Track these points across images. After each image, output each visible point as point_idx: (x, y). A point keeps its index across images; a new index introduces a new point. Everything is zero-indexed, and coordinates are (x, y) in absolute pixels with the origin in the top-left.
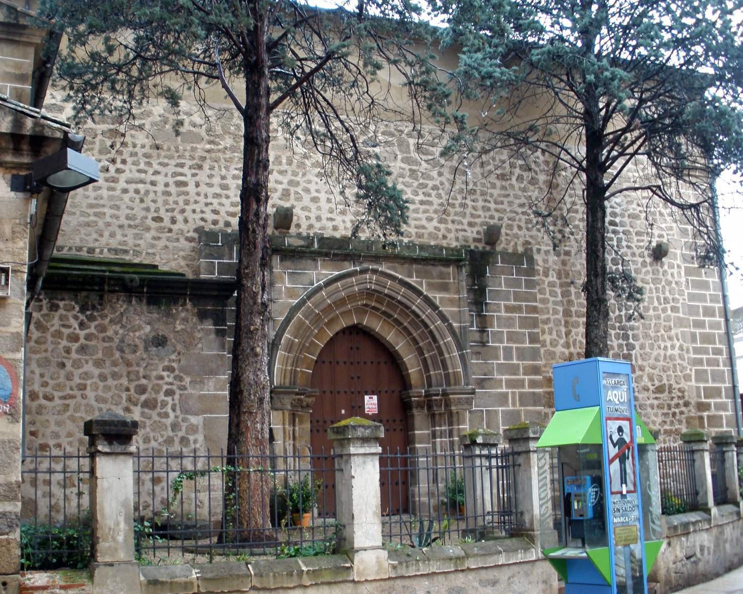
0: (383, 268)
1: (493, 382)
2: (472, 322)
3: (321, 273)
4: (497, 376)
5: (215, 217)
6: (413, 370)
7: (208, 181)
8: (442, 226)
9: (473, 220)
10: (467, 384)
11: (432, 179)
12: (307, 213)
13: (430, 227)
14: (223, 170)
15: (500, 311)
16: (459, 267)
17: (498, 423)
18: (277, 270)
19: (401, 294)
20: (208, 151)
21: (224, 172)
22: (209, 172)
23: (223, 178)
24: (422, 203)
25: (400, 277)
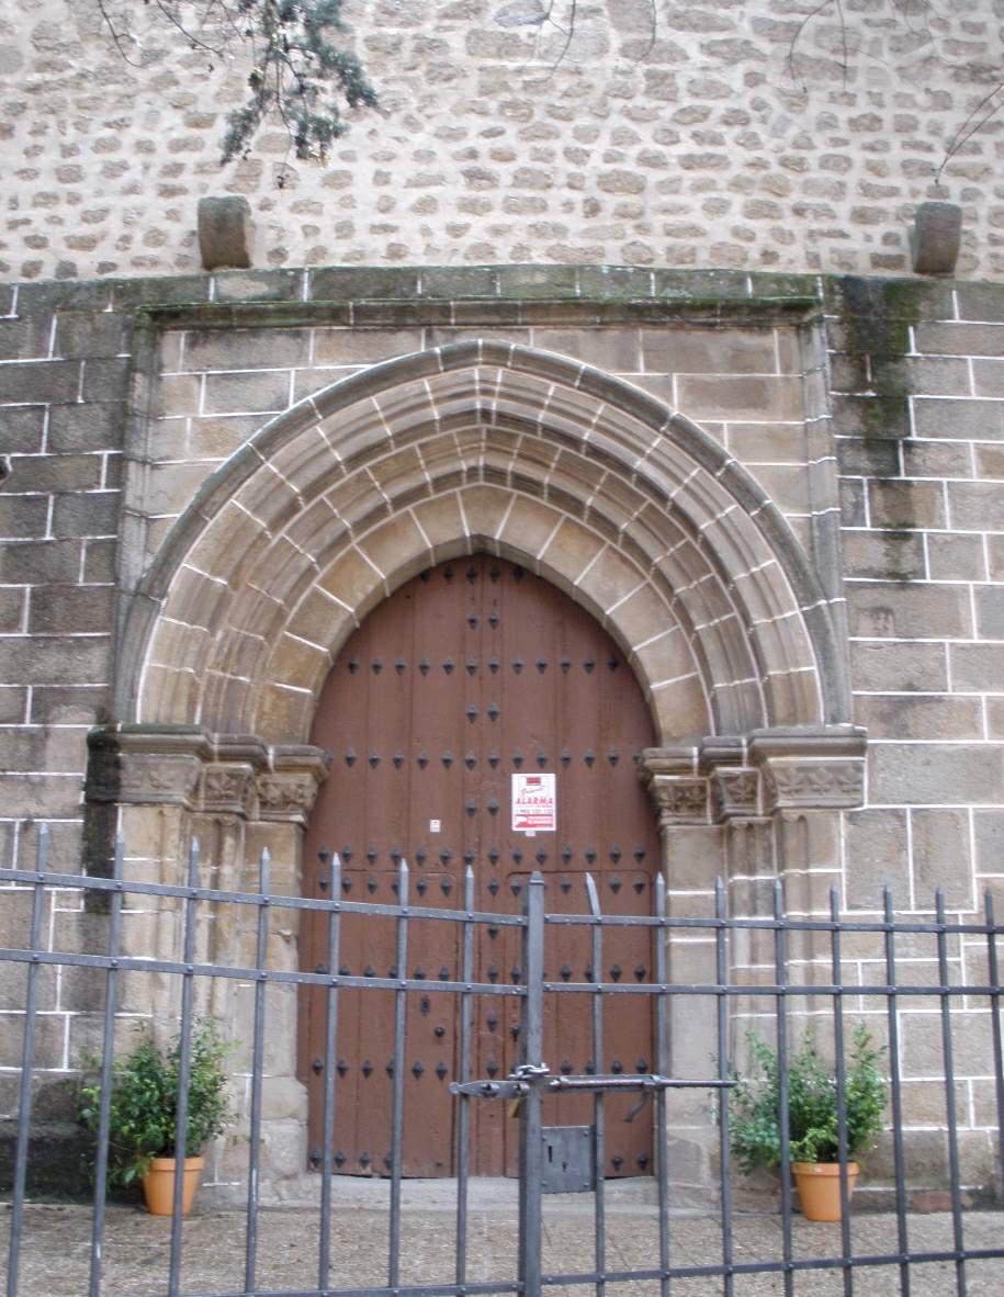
0: (533, 342)
1: (941, 710)
2: (858, 506)
3: (312, 368)
4: (955, 691)
5: (32, 255)
6: (665, 685)
7: (24, 163)
8: (760, 226)
9: (868, 203)
10: (835, 720)
11: (726, 93)
12: (308, 219)
13: (718, 230)
14: (71, 131)
15: (962, 471)
16: (803, 329)
17: (965, 863)
18: (173, 374)
19: (595, 421)
20: (34, 89)
21: (71, 135)
22: (29, 141)
23: (68, 151)
24: (689, 162)
25: (584, 365)
